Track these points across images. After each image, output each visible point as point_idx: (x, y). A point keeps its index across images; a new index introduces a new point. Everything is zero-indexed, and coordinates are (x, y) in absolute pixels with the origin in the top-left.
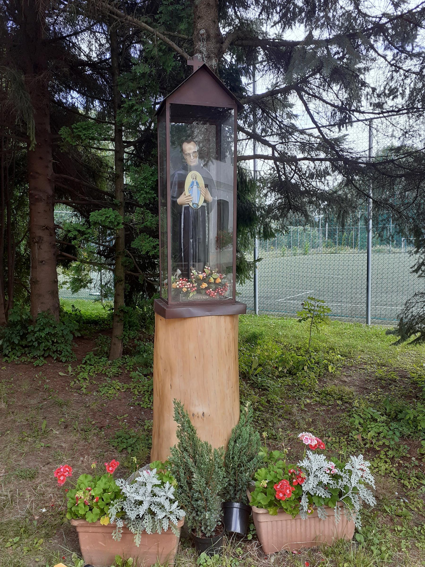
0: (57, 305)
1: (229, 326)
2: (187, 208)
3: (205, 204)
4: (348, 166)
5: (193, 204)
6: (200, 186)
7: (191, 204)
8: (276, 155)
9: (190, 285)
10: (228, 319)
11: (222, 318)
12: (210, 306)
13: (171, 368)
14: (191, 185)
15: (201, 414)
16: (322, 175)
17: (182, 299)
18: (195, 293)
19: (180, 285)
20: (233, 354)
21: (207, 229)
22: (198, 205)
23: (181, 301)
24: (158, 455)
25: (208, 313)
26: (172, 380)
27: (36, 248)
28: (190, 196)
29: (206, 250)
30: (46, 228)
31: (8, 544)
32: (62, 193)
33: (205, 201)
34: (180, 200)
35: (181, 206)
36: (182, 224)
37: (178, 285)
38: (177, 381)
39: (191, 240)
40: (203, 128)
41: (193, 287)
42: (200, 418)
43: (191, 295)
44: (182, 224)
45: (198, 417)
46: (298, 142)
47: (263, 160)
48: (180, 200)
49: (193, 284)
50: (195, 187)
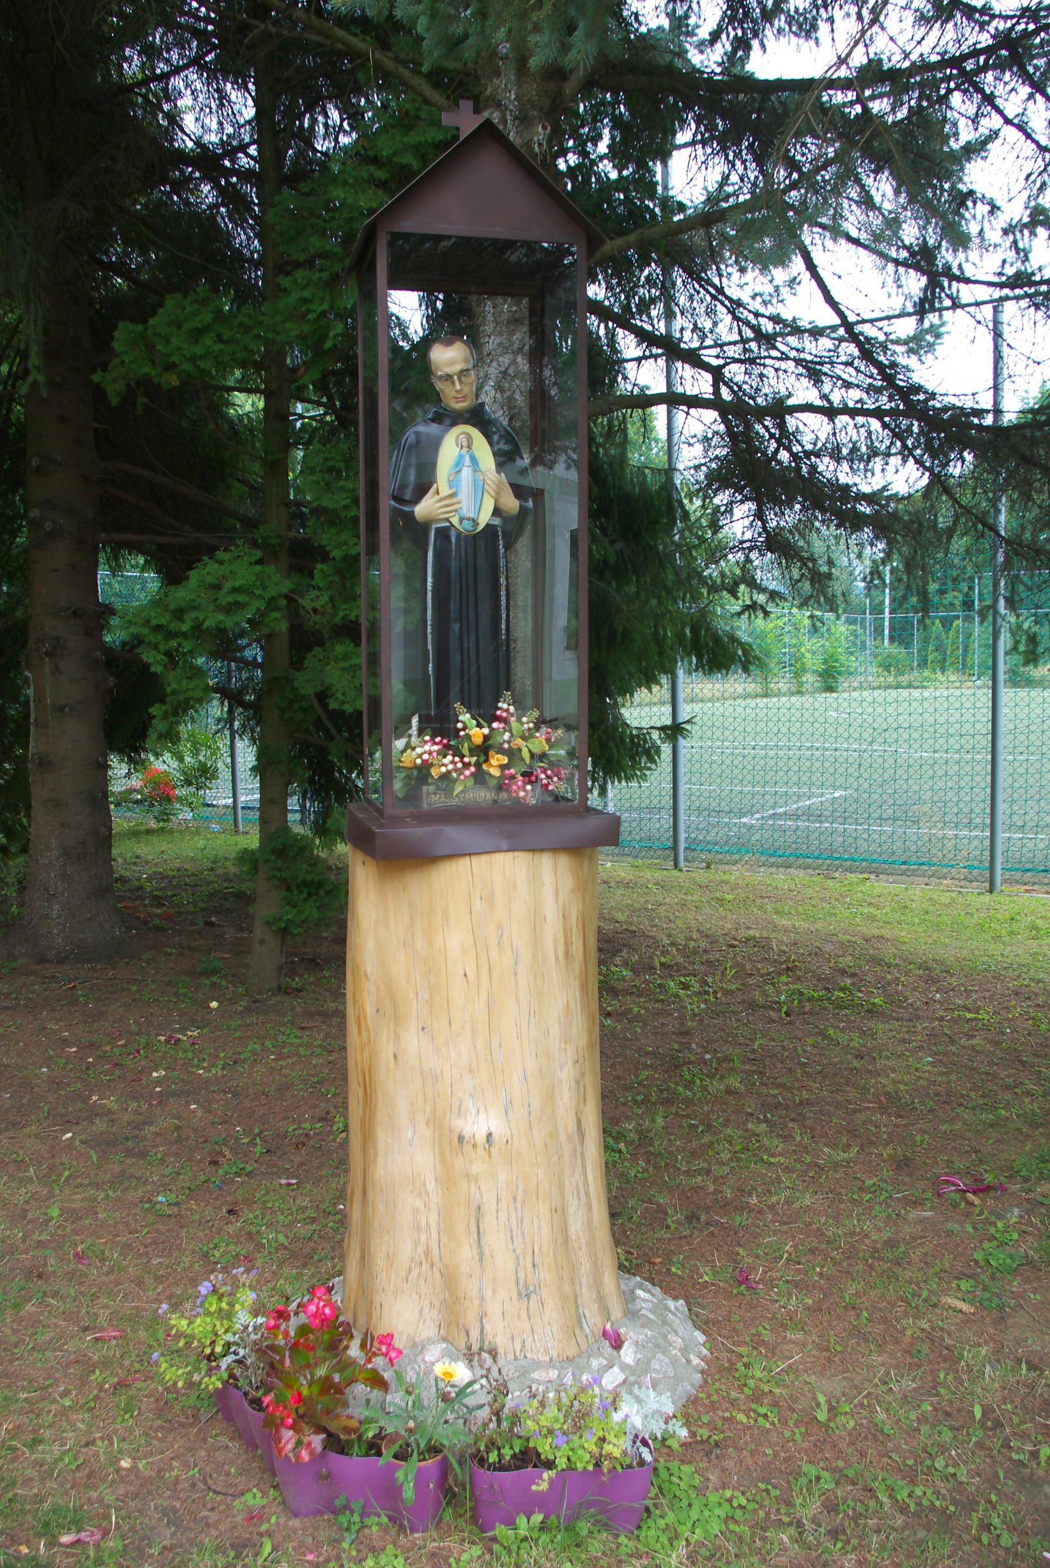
0: (103, 829)
1: (568, 881)
2: (443, 534)
3: (497, 521)
4: (939, 429)
5: (461, 520)
6: (483, 467)
7: (455, 521)
8: (726, 394)
9: (452, 762)
10: (564, 861)
11: (546, 861)
12: (512, 825)
13: (395, 1006)
14: (457, 464)
15: (481, 1138)
16: (862, 457)
17: (432, 799)
18: (471, 782)
19: (426, 757)
20: (577, 966)
21: (503, 593)
22: (475, 523)
23: (425, 806)
24: (363, 1257)
25: (504, 844)
26: (397, 1038)
27: (47, 670)
28: (452, 496)
29: (502, 654)
30: (75, 612)
31: (762, 1486)
32: (127, 520)
33: (497, 512)
34: (423, 509)
35: (425, 526)
36: (430, 580)
37: (420, 756)
38: (412, 1041)
39: (456, 627)
40: (507, 307)
41: (466, 765)
42: (480, 1150)
43: (458, 788)
44: (430, 580)
45: (475, 1146)
46: (788, 358)
47: (685, 408)
48: (423, 509)
49: (462, 757)
50: (466, 473)
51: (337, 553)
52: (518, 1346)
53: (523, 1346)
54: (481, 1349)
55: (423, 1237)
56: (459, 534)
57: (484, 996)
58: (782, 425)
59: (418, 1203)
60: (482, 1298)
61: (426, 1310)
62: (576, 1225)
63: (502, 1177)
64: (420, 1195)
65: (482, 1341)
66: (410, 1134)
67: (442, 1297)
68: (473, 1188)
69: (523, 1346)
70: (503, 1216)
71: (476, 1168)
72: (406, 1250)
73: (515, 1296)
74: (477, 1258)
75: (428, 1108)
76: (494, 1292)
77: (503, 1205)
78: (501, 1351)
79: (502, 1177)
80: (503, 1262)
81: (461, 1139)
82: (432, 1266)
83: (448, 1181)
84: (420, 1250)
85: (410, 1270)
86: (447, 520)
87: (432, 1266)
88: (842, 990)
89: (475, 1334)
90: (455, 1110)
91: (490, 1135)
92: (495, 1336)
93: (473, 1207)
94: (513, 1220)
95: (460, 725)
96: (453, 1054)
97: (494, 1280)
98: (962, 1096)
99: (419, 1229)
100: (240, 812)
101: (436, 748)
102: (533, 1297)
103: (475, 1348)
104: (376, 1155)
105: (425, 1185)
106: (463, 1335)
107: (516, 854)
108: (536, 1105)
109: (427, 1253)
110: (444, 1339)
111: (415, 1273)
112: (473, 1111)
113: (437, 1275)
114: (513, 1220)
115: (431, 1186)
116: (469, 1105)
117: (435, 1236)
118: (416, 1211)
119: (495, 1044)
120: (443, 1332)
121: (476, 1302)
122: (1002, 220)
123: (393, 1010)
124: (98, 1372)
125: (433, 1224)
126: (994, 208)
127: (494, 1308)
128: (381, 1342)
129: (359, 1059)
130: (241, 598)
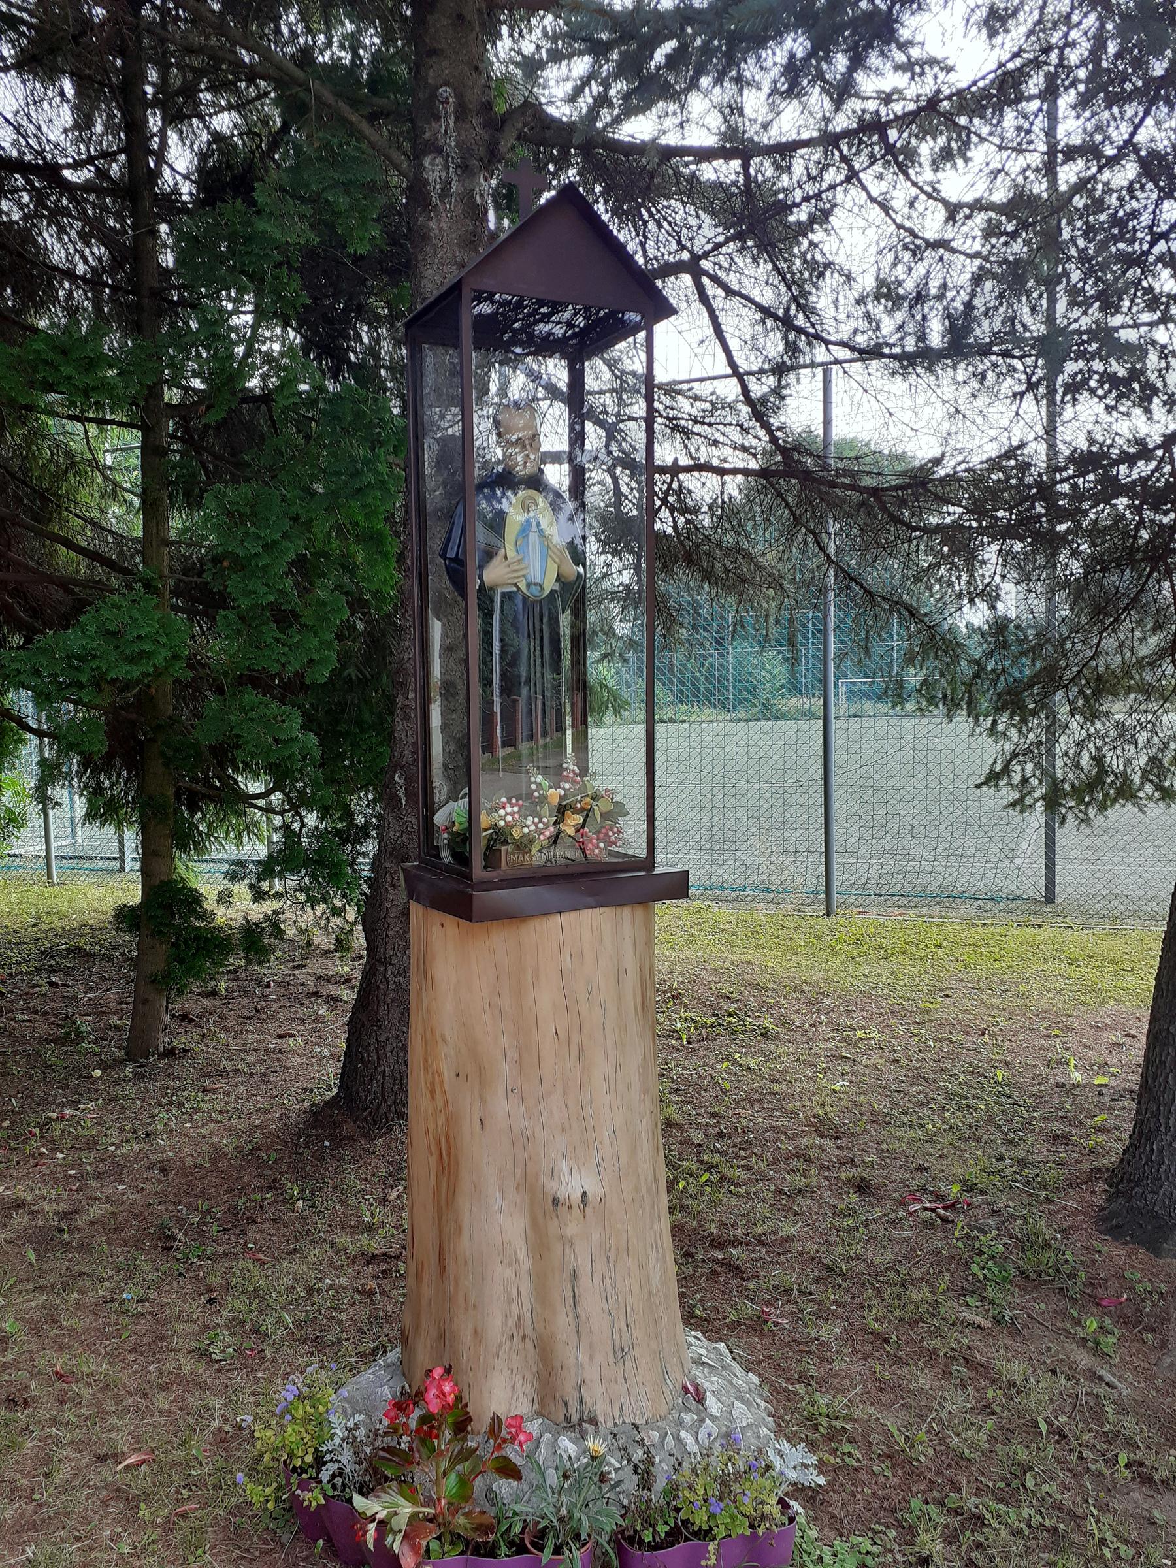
5: (528, 585)
13: (480, 1069)
19: (509, 818)
25: (590, 900)
26: (483, 1101)
38: (501, 1105)
42: (575, 1210)
51: (244, 603)
52: (617, 1412)
53: (622, 1411)
54: (581, 1420)
55: (514, 1309)
56: (525, 599)
57: (574, 1053)
58: (663, 470)
59: (509, 1273)
60: (580, 1366)
61: (518, 1385)
62: (655, 1281)
63: (596, 1237)
64: (510, 1264)
65: (582, 1410)
66: (499, 1201)
67: (534, 1369)
68: (568, 1251)
69: (622, 1411)
70: (597, 1277)
71: (571, 1230)
72: (497, 1324)
73: (611, 1359)
74: (573, 1324)
75: (518, 1172)
76: (591, 1358)
77: (597, 1266)
78: (601, 1419)
79: (596, 1237)
80: (599, 1324)
81: (556, 1201)
82: (524, 1337)
83: (540, 1245)
84: (511, 1322)
85: (501, 1345)
86: (516, 585)
87: (524, 1337)
88: (730, 1015)
89: (573, 1405)
90: (548, 1171)
91: (584, 1194)
92: (594, 1404)
93: (568, 1272)
94: (607, 1280)
95: (533, 787)
96: (545, 1114)
97: (591, 1345)
98: (886, 1115)
99: (509, 1300)
100: (54, 863)
101: (516, 809)
102: (628, 1358)
103: (574, 1420)
104: (459, 1229)
105: (515, 1253)
106: (561, 1406)
107: (602, 910)
108: (624, 1160)
109: (519, 1325)
110: (540, 1414)
111: (506, 1348)
112: (566, 1171)
113: (530, 1346)
114: (607, 1280)
115: (522, 1254)
116: (563, 1164)
117: (526, 1306)
118: (506, 1281)
119: (586, 1100)
120: (536, 1406)
121: (574, 1371)
122: (857, 290)
123: (478, 1072)
124: (143, 1506)
125: (524, 1293)
126: (849, 278)
127: (591, 1374)
128: (510, 1426)
129: (431, 1126)
130: (147, 647)
